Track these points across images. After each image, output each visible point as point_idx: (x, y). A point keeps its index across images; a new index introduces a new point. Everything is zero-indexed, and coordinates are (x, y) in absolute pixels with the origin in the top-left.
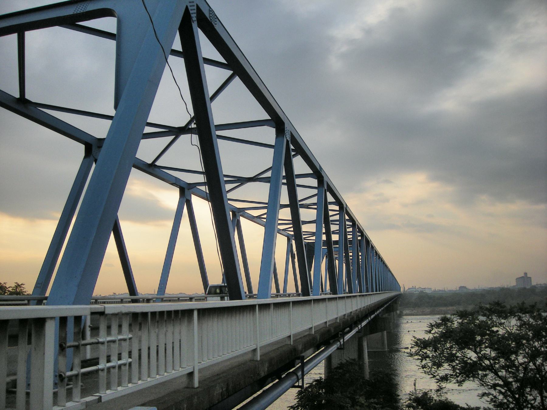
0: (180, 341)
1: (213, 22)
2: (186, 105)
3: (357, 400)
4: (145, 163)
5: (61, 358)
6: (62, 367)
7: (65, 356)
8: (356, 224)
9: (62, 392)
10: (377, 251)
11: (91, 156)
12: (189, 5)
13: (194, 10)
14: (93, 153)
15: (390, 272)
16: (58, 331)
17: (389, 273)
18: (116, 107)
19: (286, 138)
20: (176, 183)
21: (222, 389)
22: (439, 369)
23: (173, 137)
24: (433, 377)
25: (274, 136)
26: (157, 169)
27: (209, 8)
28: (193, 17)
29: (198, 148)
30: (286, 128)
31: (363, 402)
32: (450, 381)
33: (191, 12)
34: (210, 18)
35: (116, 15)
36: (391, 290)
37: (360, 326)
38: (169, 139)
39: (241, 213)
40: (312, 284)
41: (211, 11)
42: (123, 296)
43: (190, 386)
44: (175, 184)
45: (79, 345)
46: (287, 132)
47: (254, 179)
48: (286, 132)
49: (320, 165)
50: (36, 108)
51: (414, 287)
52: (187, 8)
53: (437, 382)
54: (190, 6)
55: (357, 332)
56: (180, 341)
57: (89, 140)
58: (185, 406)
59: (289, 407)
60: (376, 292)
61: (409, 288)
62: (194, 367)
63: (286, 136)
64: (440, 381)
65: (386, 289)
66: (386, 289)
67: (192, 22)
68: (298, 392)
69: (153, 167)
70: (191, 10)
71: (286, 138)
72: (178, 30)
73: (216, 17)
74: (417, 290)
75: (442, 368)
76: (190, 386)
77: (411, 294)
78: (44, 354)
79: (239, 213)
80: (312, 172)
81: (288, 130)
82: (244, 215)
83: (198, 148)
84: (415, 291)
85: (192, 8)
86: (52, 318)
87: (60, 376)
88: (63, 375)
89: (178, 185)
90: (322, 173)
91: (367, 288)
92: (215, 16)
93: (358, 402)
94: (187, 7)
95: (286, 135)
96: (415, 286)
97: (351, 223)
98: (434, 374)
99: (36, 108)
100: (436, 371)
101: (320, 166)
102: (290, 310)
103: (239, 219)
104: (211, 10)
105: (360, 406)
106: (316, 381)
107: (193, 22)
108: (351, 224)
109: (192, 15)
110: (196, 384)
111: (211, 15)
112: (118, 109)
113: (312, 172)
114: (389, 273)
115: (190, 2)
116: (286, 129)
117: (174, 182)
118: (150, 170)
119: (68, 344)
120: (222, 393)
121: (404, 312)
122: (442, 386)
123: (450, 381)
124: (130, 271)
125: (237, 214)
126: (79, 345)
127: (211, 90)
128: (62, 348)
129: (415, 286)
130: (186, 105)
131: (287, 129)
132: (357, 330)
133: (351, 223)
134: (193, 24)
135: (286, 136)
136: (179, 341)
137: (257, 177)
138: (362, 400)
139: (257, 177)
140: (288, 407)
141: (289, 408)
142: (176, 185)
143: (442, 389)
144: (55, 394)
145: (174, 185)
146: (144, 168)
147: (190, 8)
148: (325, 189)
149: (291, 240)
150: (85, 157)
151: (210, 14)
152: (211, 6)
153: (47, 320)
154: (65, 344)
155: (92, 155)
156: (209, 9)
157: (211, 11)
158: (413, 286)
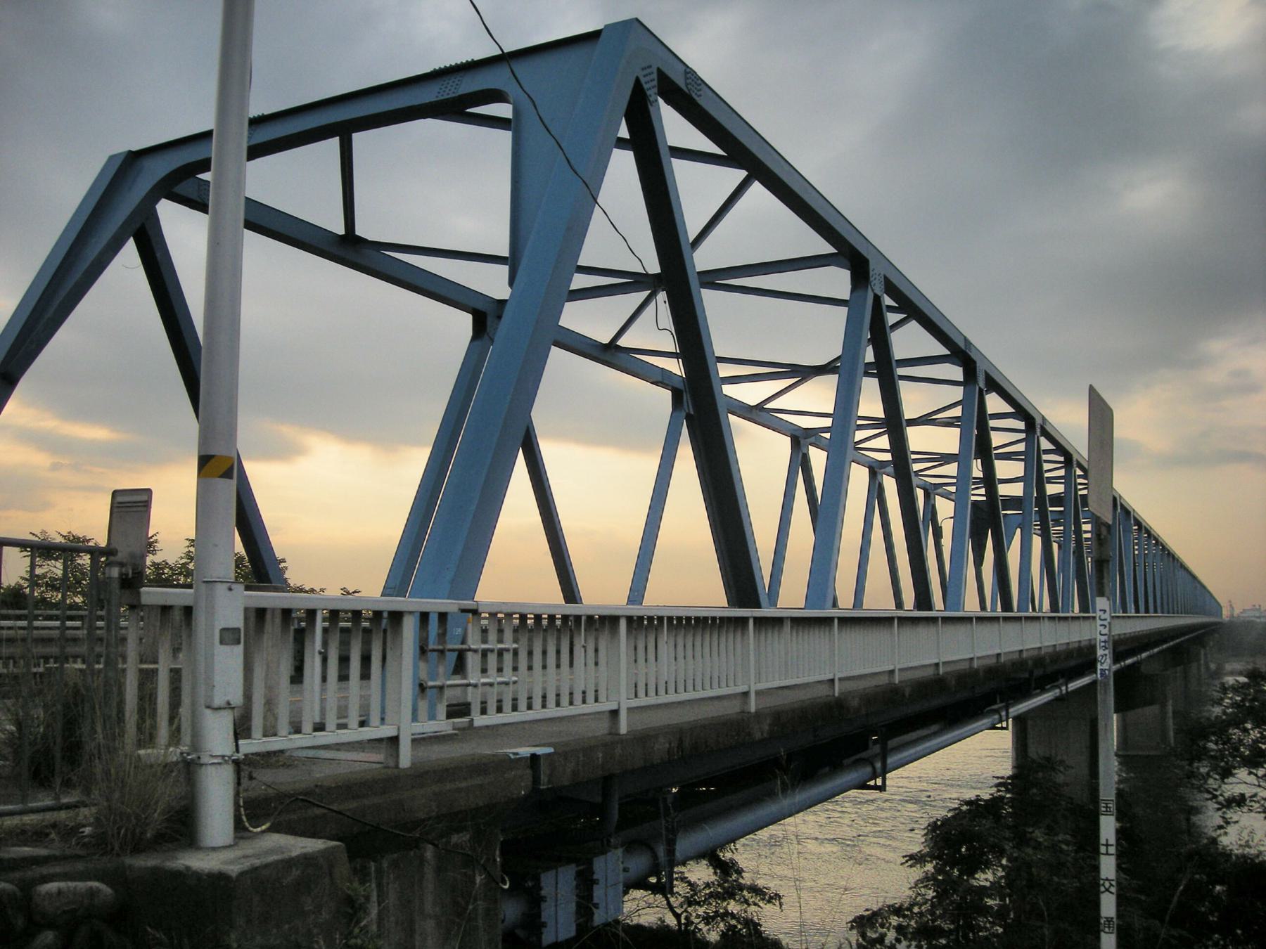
0: (636, 687)
1: (693, 95)
2: (641, 262)
3: (1028, 835)
4: (592, 342)
5: (422, 665)
6: (423, 675)
7: (427, 661)
8: (1074, 459)
9: (423, 706)
10: (1141, 521)
11: (486, 335)
12: (641, 75)
13: (653, 80)
14: (488, 329)
15: (1183, 567)
16: (418, 629)
17: (1180, 573)
18: (511, 283)
19: (873, 290)
20: (665, 381)
21: (670, 744)
22: (1226, 780)
23: (647, 293)
24: (1211, 799)
25: (849, 287)
26: (623, 355)
27: (684, 68)
28: (650, 96)
29: (672, 334)
30: (873, 271)
31: (1041, 840)
32: (1251, 808)
33: (646, 87)
34: (687, 88)
35: (512, 101)
36: (1210, 615)
37: (1064, 688)
38: (641, 296)
39: (812, 439)
40: (1058, 603)
41: (688, 73)
42: (809, 696)
43: (614, 732)
44: (661, 382)
45: (444, 649)
46: (875, 279)
47: (830, 367)
48: (871, 279)
49: (965, 337)
50: (379, 251)
51: (1257, 607)
52: (638, 81)
53: (1218, 809)
54: (645, 76)
55: (1057, 699)
56: (636, 687)
57: (480, 306)
58: (601, 755)
59: (906, 856)
60: (1146, 613)
61: (1244, 610)
62: (619, 704)
63: (872, 288)
64: (1224, 806)
65: (1173, 609)
66: (1168, 609)
67: (649, 104)
68: (929, 825)
69: (613, 351)
70: (646, 83)
71: (873, 290)
72: (624, 122)
73: (700, 82)
74: (1263, 615)
75: (1231, 780)
76: (614, 732)
77: (1248, 625)
78: (401, 654)
79: (807, 440)
80: (949, 353)
81: (878, 274)
82: (818, 443)
83: (672, 334)
84: (1259, 617)
85: (648, 78)
86: (411, 613)
87: (421, 685)
88: (424, 684)
89: (667, 385)
90: (970, 354)
91: (1155, 607)
92: (698, 80)
93: (1031, 839)
94: (638, 81)
95: (872, 284)
96: (1260, 606)
97: (1063, 458)
98: (1215, 793)
99: (379, 251)
100: (1220, 787)
101: (966, 339)
102: (832, 633)
103: (806, 452)
104: (688, 70)
105: (1035, 848)
106: (969, 803)
107: (651, 105)
108: (1062, 459)
109: (648, 93)
110: (623, 729)
111: (689, 81)
112: (514, 285)
113: (949, 353)
114: (1180, 574)
115: (643, 69)
116: (871, 273)
117: (660, 379)
118: (607, 357)
119: (431, 646)
120: (669, 749)
121: (1228, 667)
122: (1231, 818)
123: (1251, 808)
124: (568, 562)
125: (802, 442)
126: (444, 649)
127: (693, 225)
128: (423, 651)
129: (1260, 606)
130: (641, 262)
131: (875, 272)
132: (1058, 694)
133: (1063, 458)
134: (650, 107)
135: (872, 288)
136: (634, 686)
137: (833, 365)
138: (1039, 835)
139: (833, 365)
140: (904, 857)
141: (907, 858)
142: (663, 386)
143: (1228, 823)
144: (415, 711)
145: (659, 384)
146: (595, 354)
147: (643, 80)
148: (980, 388)
149: (932, 496)
150: (474, 338)
151: (686, 79)
152: (687, 63)
153: (405, 614)
154: (427, 646)
155: (488, 334)
156: (685, 70)
157: (688, 73)
158: (1254, 606)
